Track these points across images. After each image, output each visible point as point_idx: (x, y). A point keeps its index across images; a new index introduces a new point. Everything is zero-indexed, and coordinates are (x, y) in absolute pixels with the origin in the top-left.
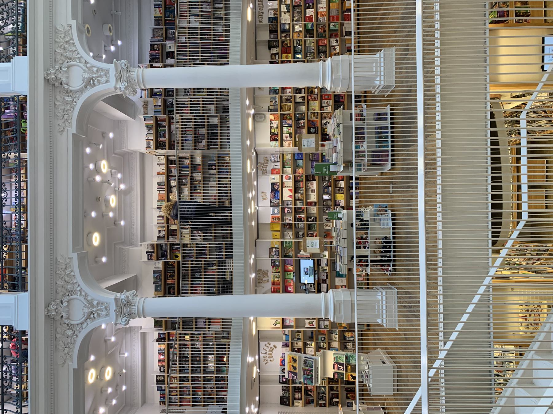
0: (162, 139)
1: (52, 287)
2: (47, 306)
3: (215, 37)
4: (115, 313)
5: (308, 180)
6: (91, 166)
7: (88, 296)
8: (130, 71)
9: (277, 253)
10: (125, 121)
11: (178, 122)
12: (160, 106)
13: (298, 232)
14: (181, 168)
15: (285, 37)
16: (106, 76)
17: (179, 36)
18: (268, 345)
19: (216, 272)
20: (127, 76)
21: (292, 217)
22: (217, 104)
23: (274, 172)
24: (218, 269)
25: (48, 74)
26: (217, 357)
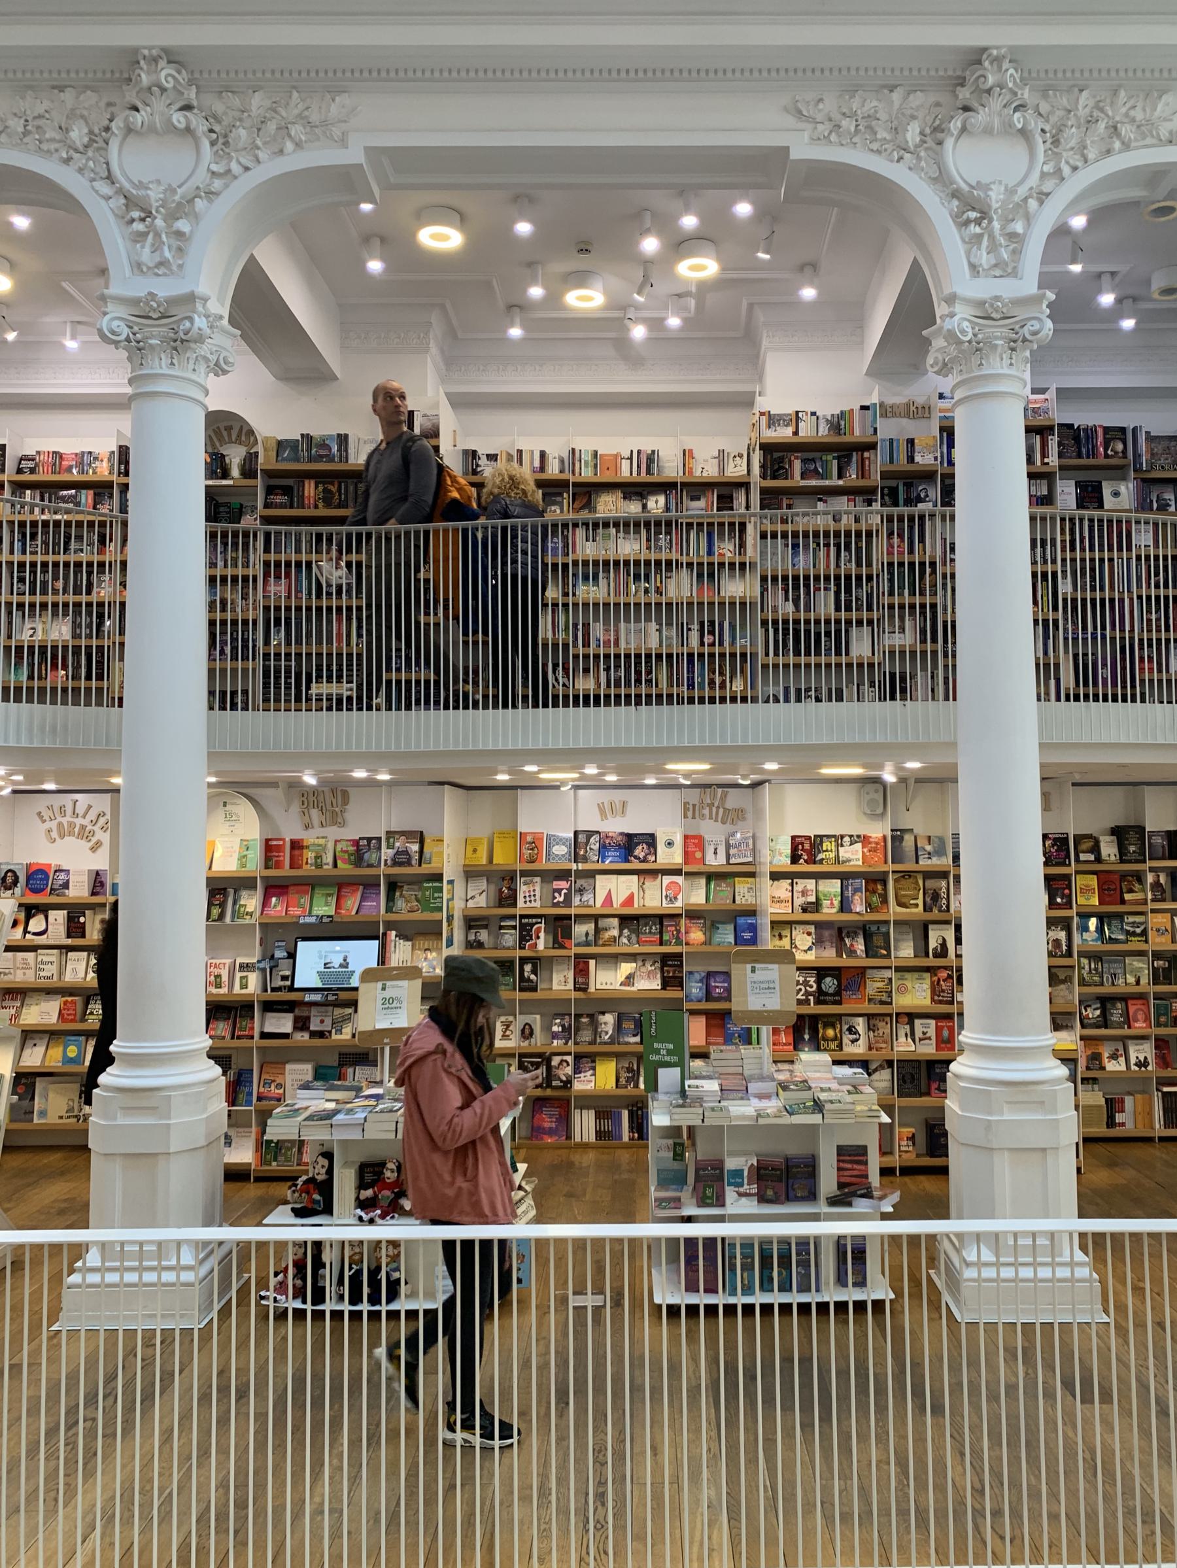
0: (797, 466)
1: (241, 75)
2: (173, 57)
3: (1150, 645)
4: (142, 294)
5: (664, 964)
6: (689, 222)
7: (210, 201)
8: (1013, 349)
9: (403, 858)
10: (861, 344)
11: (857, 520)
12: (911, 459)
13: (486, 927)
14: (710, 531)
15: (1156, 885)
16: (996, 266)
17: (1156, 525)
18: (102, 821)
19: (339, 648)
20: (997, 338)
21: (538, 904)
22: (924, 653)
23: (694, 844)
24: (350, 655)
25: (997, 60)
26: (65, 648)
